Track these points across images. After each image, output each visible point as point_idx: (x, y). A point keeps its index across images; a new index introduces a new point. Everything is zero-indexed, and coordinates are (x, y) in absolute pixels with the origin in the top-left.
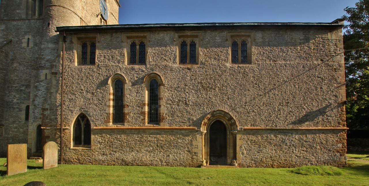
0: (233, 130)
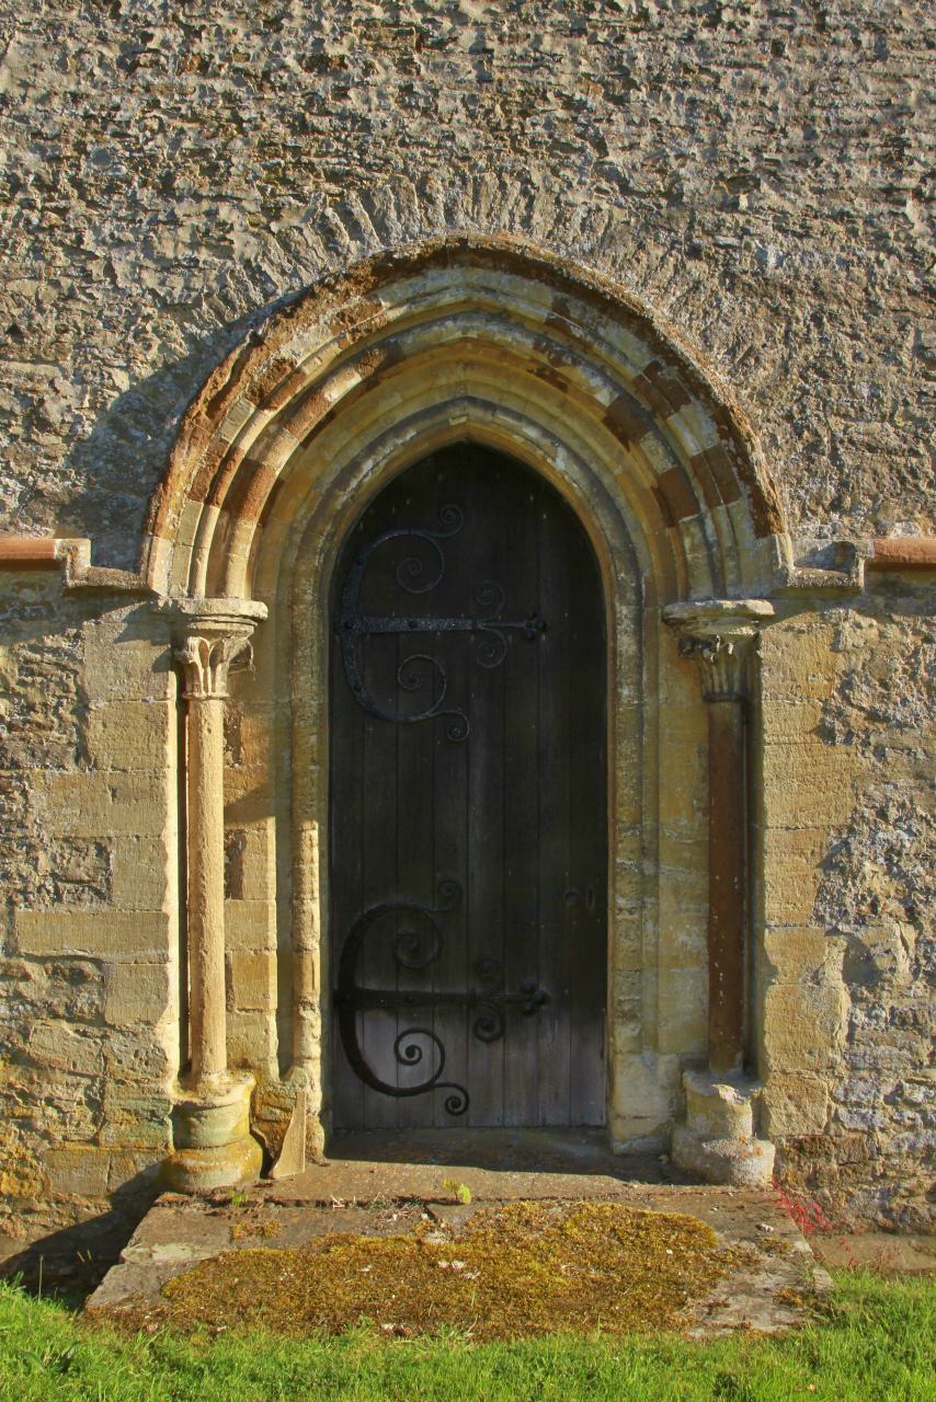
0: (703, 586)
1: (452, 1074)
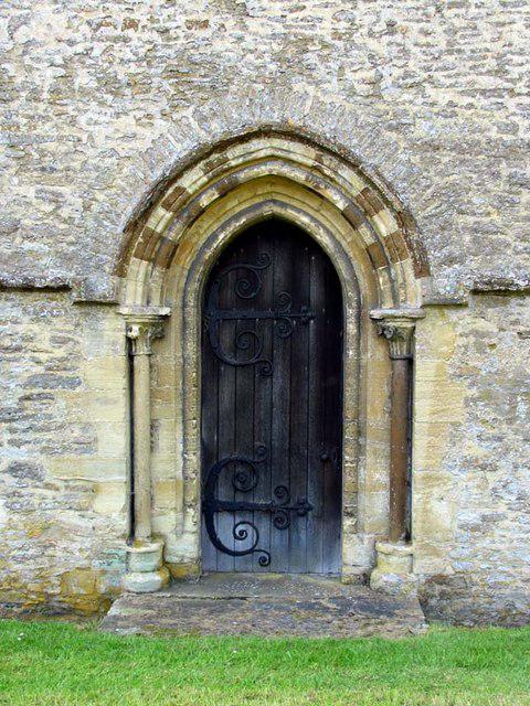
1: (262, 545)
